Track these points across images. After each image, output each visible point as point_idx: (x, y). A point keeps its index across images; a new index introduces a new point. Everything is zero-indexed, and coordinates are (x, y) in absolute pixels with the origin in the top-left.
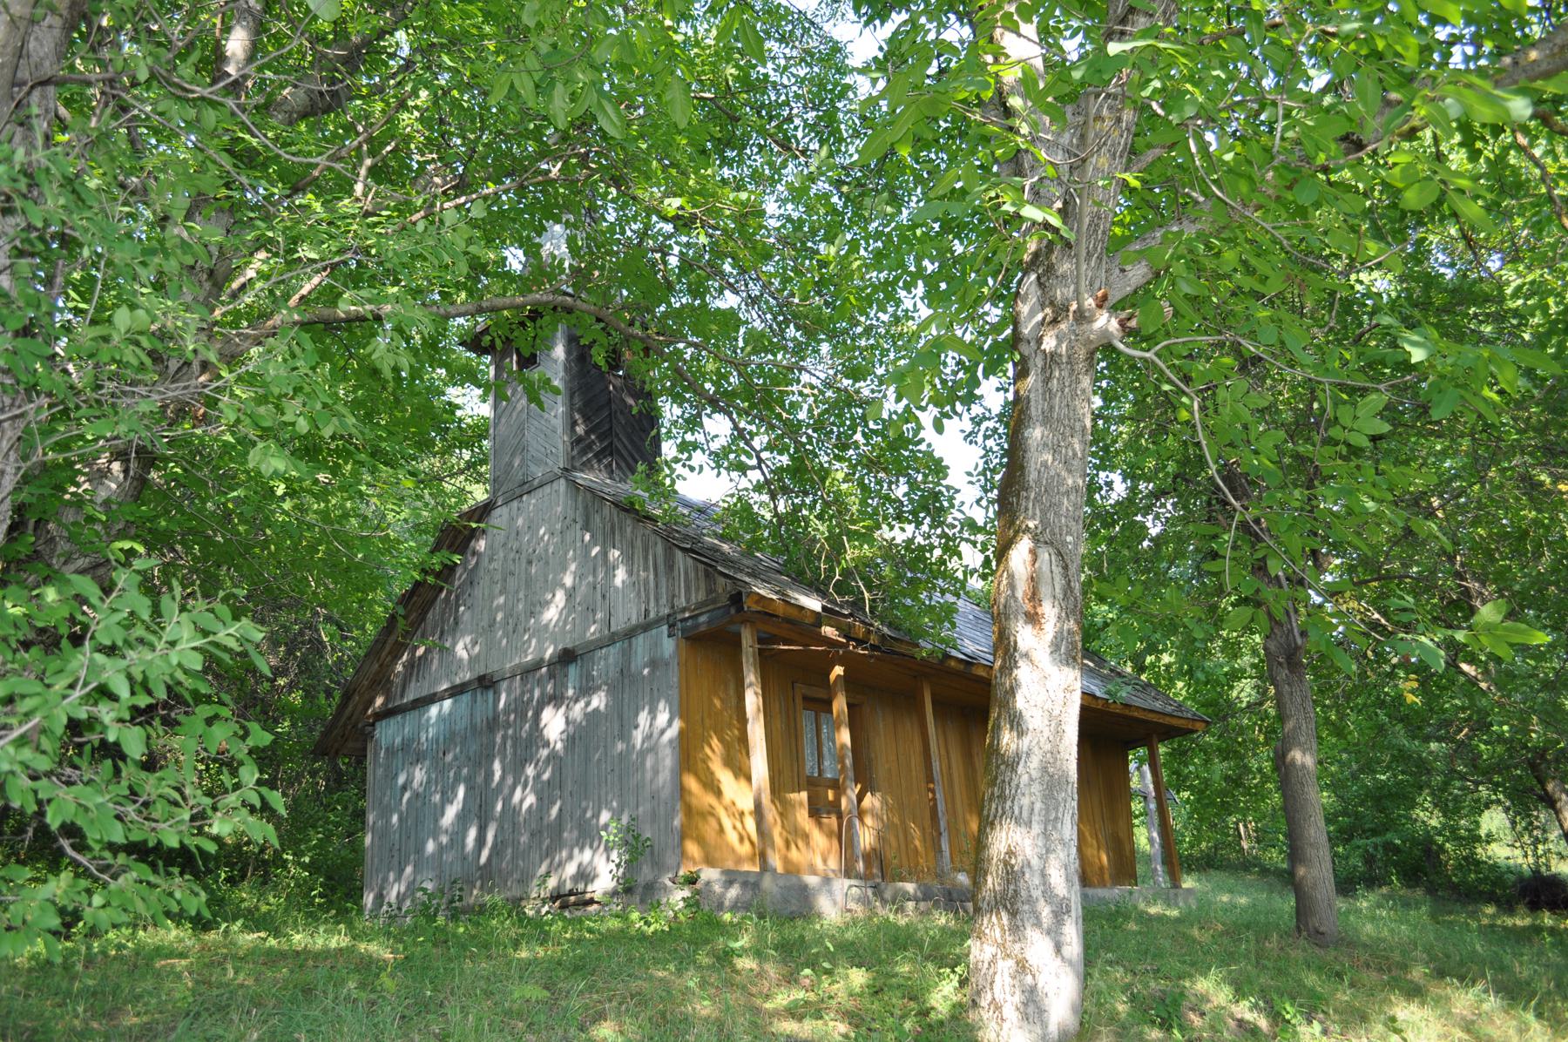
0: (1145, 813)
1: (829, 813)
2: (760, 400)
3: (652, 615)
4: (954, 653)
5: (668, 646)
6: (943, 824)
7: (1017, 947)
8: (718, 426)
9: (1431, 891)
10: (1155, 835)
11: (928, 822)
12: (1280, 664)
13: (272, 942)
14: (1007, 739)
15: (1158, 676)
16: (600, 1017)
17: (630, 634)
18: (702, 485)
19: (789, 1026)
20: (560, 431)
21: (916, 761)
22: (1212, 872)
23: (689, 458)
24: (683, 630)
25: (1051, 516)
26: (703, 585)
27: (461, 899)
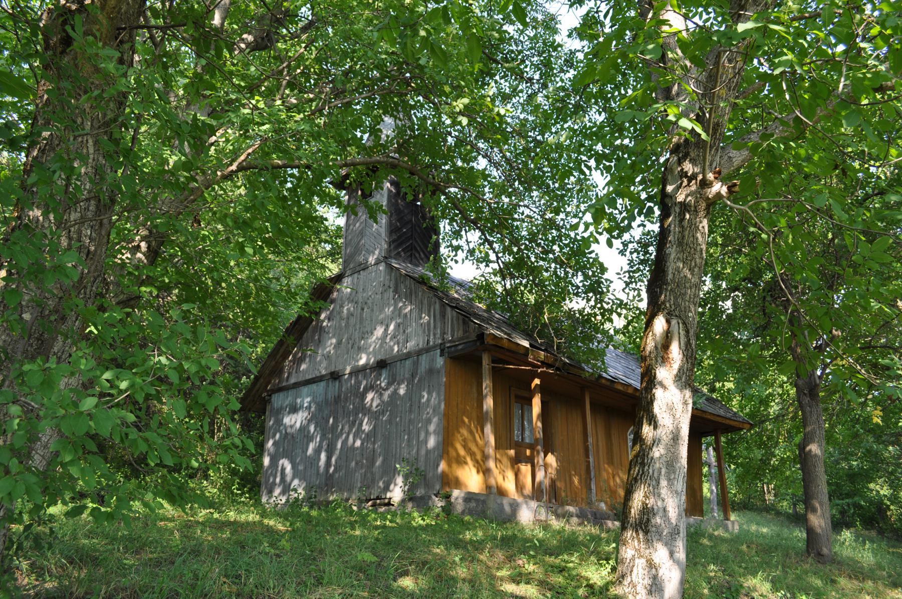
0: (710, 474)
1: (526, 462)
2: (497, 223)
3: (431, 343)
4: (604, 375)
5: (440, 362)
6: (592, 474)
7: (648, 551)
8: (474, 236)
9: (881, 532)
10: (714, 488)
11: (583, 472)
12: (805, 394)
13: (216, 516)
14: (647, 431)
15: (722, 396)
16: (406, 573)
17: (419, 353)
18: (463, 271)
19: (510, 588)
20: (383, 235)
21: (578, 437)
22: (748, 512)
23: (456, 255)
24: (449, 353)
25: (680, 300)
26: (461, 328)
27: (315, 497)
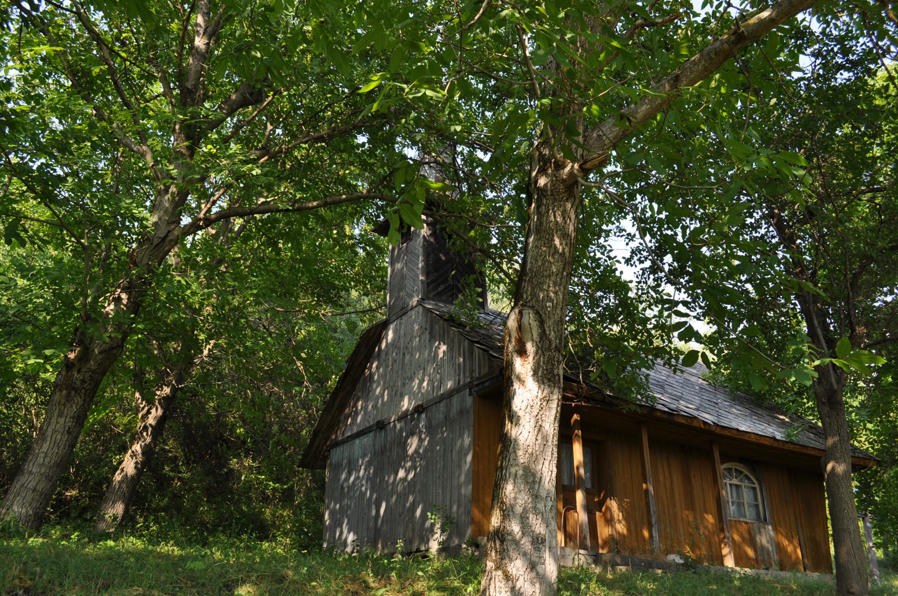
5: (469, 400)
12: (823, 403)
